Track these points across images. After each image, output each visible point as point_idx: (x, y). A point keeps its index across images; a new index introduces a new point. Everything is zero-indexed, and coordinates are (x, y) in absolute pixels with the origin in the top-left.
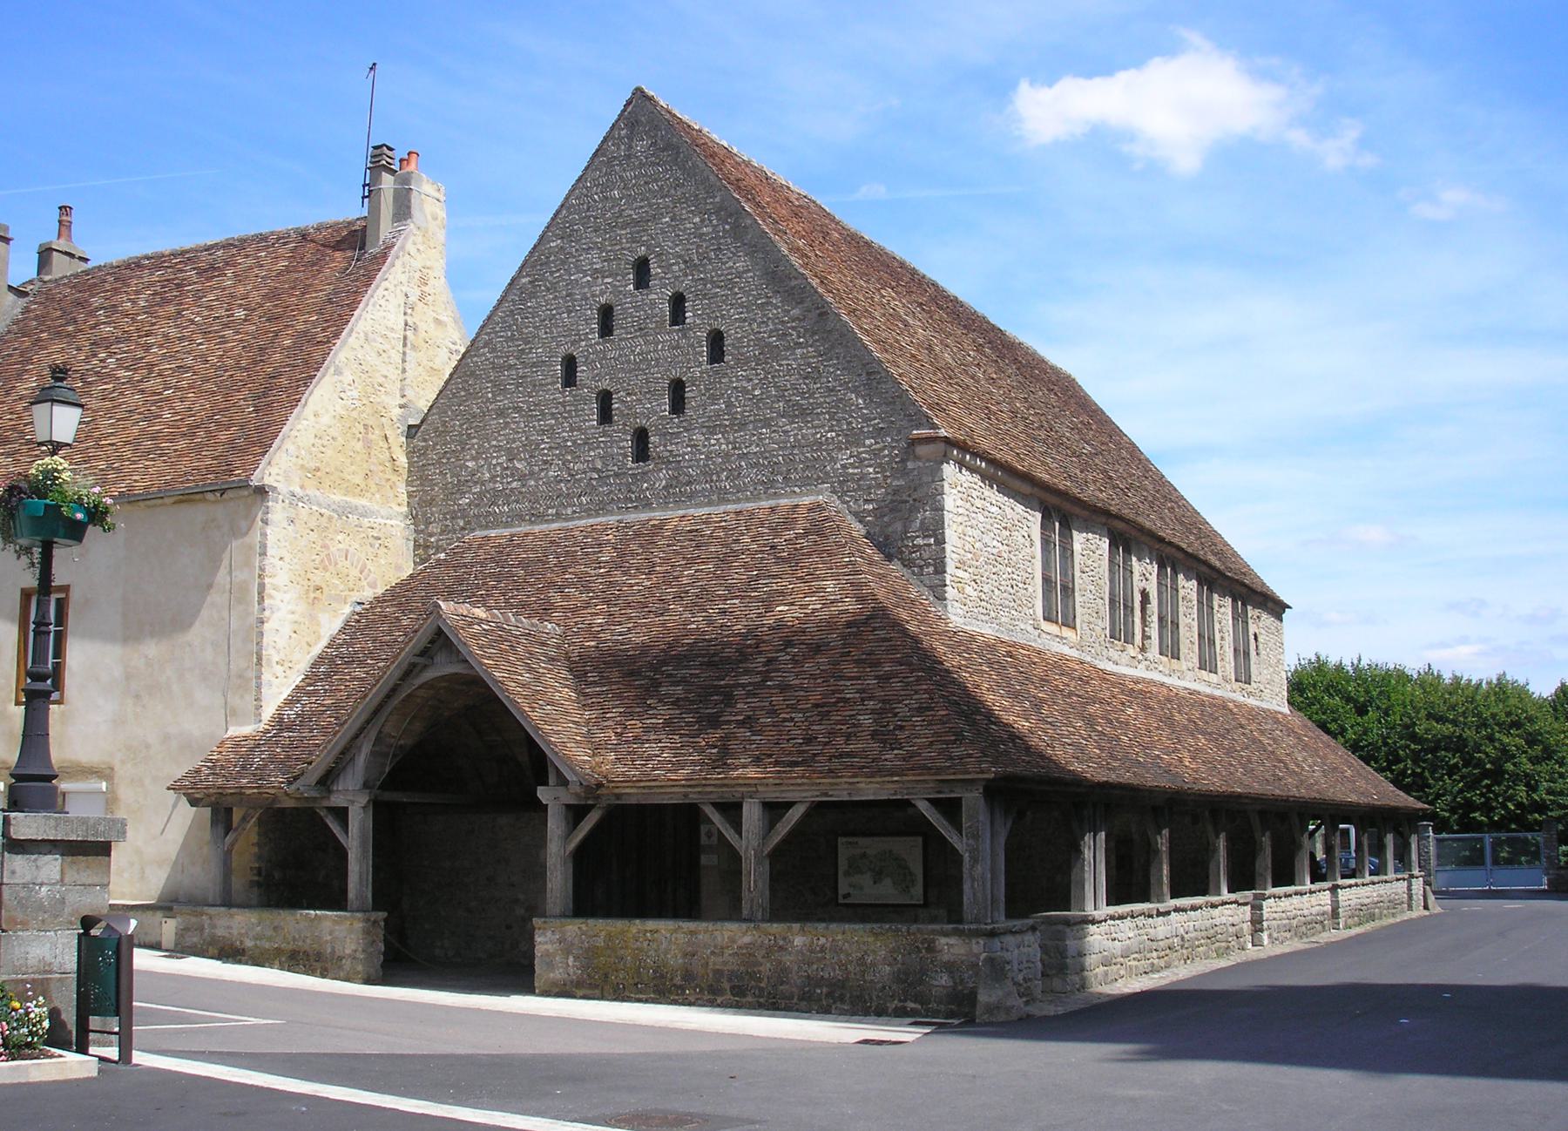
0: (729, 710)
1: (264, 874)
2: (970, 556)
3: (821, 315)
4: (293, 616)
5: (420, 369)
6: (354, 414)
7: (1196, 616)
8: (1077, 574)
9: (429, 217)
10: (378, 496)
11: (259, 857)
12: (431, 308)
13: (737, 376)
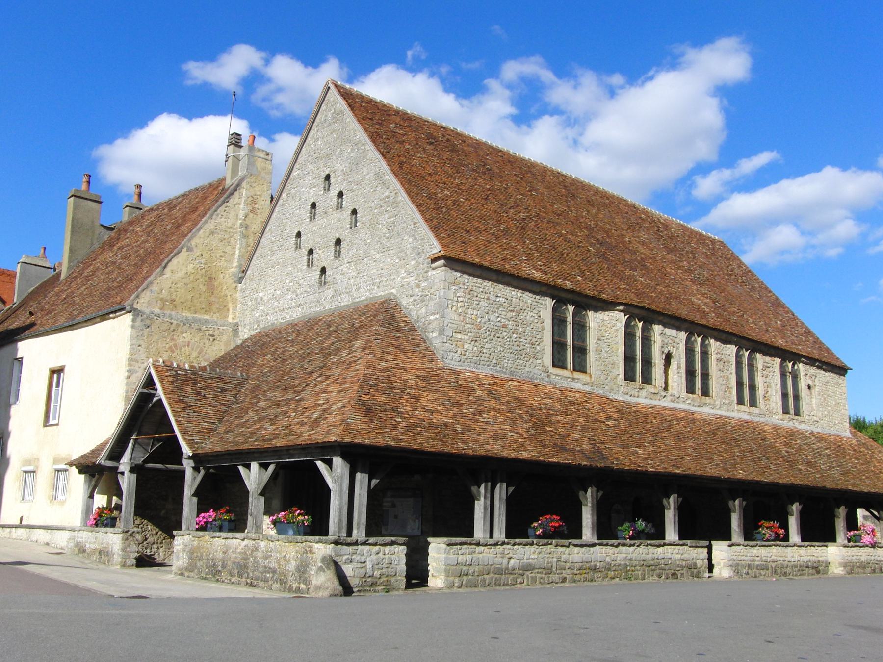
3: (396, 194)
13: (363, 233)
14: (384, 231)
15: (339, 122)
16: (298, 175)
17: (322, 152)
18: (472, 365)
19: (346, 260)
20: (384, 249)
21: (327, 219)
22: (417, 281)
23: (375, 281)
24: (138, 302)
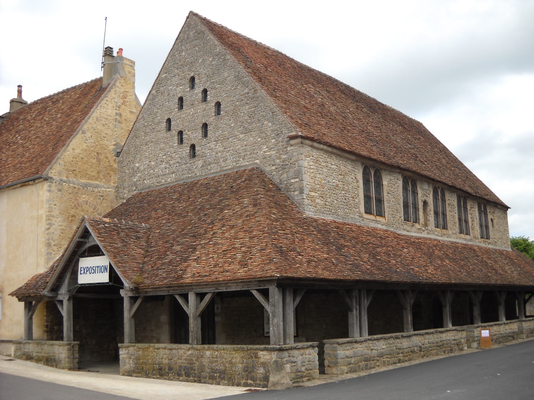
0: (192, 254)
1: (49, 326)
2: (318, 186)
3: (255, 91)
4: (61, 227)
5: (123, 131)
6: (92, 149)
7: (456, 212)
8: (385, 194)
9: (127, 73)
10: (104, 180)
11: (47, 321)
12: (128, 107)
14: (245, 117)
15: (201, 39)
16: (166, 77)
17: (186, 61)
18: (321, 214)
19: (213, 139)
20: (247, 131)
21: (193, 109)
22: (278, 154)
23: (240, 155)
24: (51, 173)
